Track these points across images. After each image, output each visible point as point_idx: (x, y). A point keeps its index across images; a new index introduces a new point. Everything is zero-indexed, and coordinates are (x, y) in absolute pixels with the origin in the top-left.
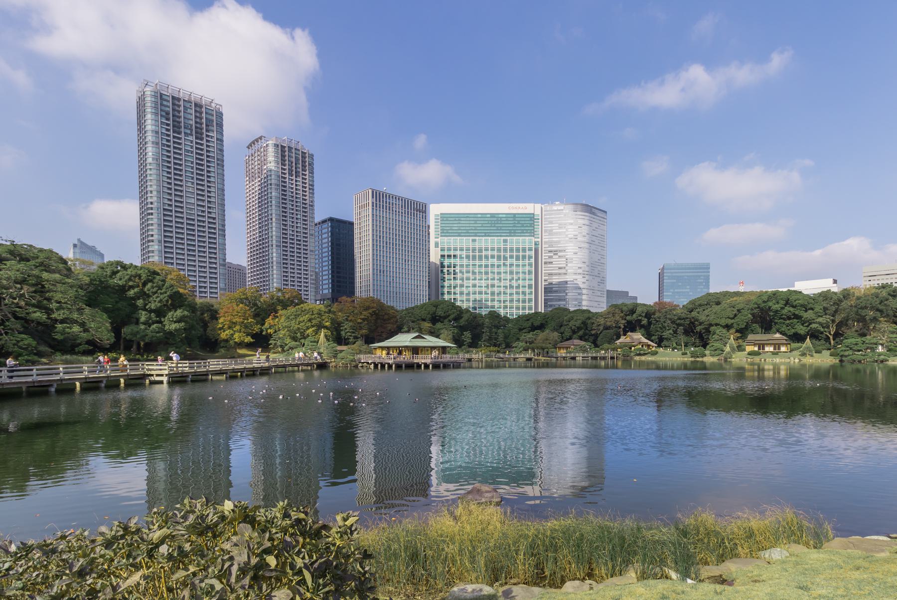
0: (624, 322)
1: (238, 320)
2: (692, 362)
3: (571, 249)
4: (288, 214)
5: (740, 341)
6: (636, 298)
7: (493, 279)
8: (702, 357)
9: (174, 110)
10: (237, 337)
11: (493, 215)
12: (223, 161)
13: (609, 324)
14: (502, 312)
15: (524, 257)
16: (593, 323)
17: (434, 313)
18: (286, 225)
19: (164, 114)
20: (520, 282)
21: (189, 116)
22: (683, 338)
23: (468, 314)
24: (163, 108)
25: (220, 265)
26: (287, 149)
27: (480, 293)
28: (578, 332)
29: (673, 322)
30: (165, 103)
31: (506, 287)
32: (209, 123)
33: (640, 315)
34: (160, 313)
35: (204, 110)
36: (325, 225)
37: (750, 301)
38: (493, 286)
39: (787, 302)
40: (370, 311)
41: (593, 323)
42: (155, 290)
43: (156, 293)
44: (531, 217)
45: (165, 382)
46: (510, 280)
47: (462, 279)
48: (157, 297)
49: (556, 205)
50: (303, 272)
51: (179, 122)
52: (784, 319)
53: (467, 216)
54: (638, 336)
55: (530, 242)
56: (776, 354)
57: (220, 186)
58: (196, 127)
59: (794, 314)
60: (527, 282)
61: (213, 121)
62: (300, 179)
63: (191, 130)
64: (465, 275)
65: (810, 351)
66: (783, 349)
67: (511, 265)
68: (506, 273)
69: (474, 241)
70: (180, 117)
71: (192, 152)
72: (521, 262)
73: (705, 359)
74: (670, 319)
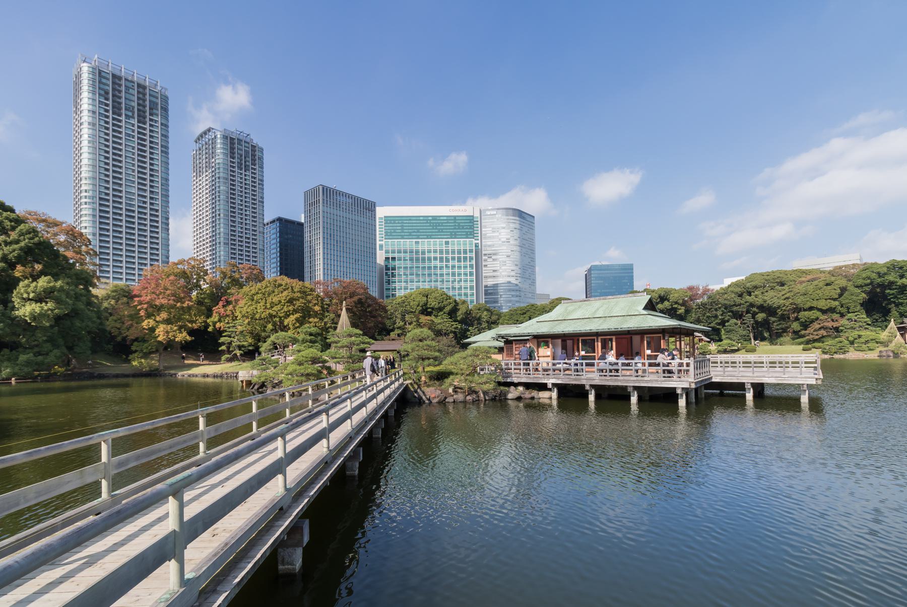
1: (164, 301)
4: (236, 210)
7: (436, 281)
8: (844, 353)
9: (114, 89)
10: (161, 334)
11: (435, 218)
17: (426, 304)
18: (234, 222)
19: (102, 92)
20: (463, 284)
21: (132, 97)
23: (465, 306)
24: (102, 86)
26: (236, 141)
30: (104, 81)
32: (153, 106)
35: (147, 91)
40: (356, 298)
44: (471, 220)
47: (406, 282)
55: (471, 244)
57: (164, 176)
58: (139, 110)
60: (469, 284)
61: (157, 104)
63: (133, 112)
67: (453, 267)
68: (448, 274)
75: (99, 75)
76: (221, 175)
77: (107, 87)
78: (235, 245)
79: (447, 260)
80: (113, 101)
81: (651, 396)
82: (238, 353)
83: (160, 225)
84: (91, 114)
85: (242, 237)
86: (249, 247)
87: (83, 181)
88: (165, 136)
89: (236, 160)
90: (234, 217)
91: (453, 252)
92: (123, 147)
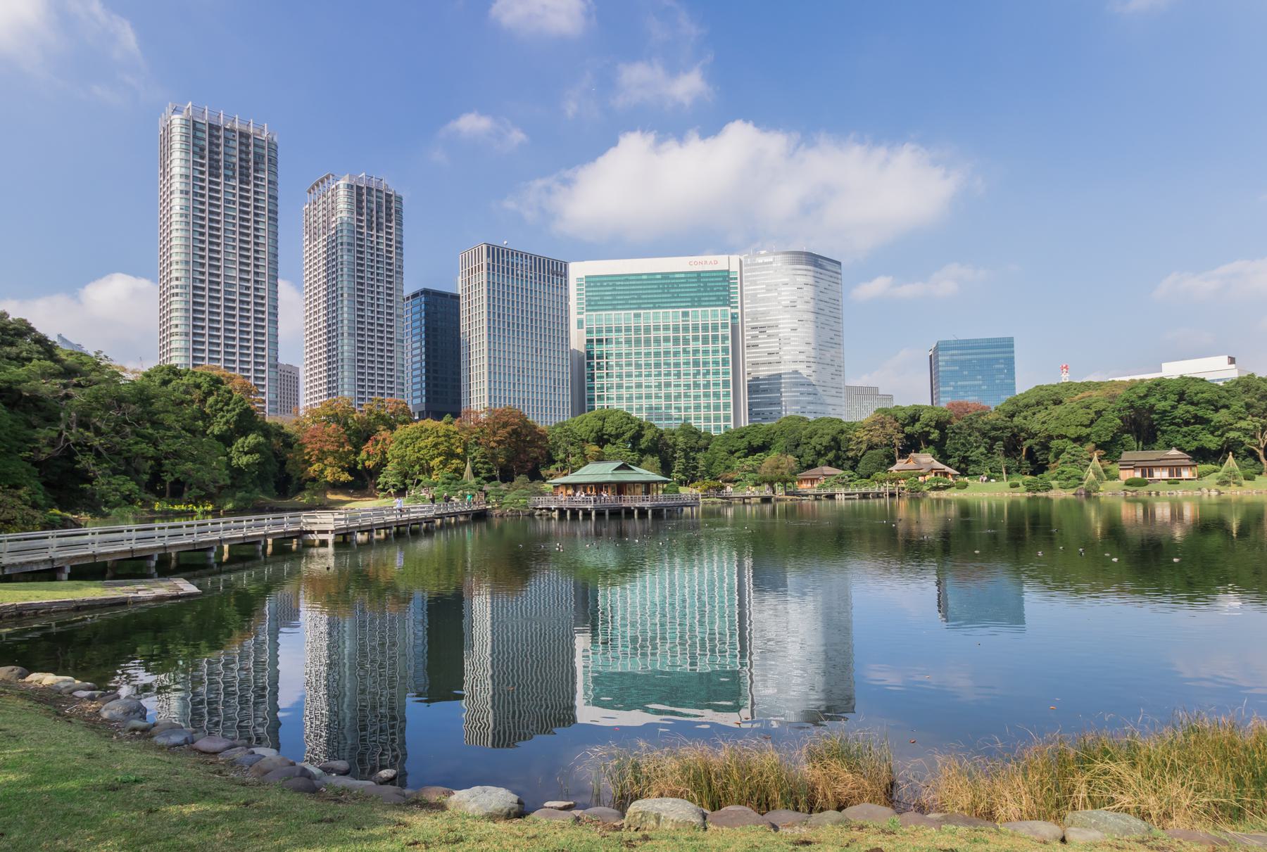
0: (901, 436)
2: (1029, 499)
3: (786, 322)
4: (366, 287)
5: (1105, 462)
6: (890, 397)
7: (668, 374)
8: (1047, 490)
9: (211, 143)
10: (329, 475)
11: (665, 276)
12: (276, 213)
13: (875, 440)
14: (701, 425)
15: (715, 338)
16: (850, 440)
17: (601, 430)
19: (197, 150)
20: (711, 378)
22: (1002, 461)
23: (652, 431)
24: (197, 142)
25: (270, 366)
26: (364, 191)
27: (649, 397)
28: (825, 454)
29: (984, 435)
30: (199, 134)
31: (688, 386)
33: (927, 425)
34: (226, 439)
35: (251, 141)
37: (1114, 397)
38: (668, 385)
39: (1181, 397)
40: (509, 429)
41: (850, 440)
42: (220, 405)
43: (221, 410)
44: (725, 276)
45: (330, 543)
46: (695, 375)
47: (620, 376)
48: (222, 417)
49: (760, 255)
50: (386, 372)
51: (218, 161)
52: (1178, 425)
53: (626, 278)
54: (926, 458)
55: (724, 315)
56: (1176, 482)
58: (241, 167)
59: (1195, 417)
60: (721, 378)
62: (383, 234)
64: (625, 369)
65: (1235, 477)
66: (1186, 474)
67: (696, 352)
68: (687, 363)
70: (218, 153)
72: (710, 347)
73: (1051, 494)
74: (979, 430)
75: (193, 127)
76: (345, 239)
77: (202, 143)
78: (363, 336)
79: (686, 341)
80: (210, 159)
81: (908, 542)
82: (392, 491)
84: (183, 180)
85: (372, 324)
86: (382, 332)
87: (174, 267)
88: (273, 198)
89: (364, 218)
90: (362, 297)
91: (695, 328)
92: (221, 218)
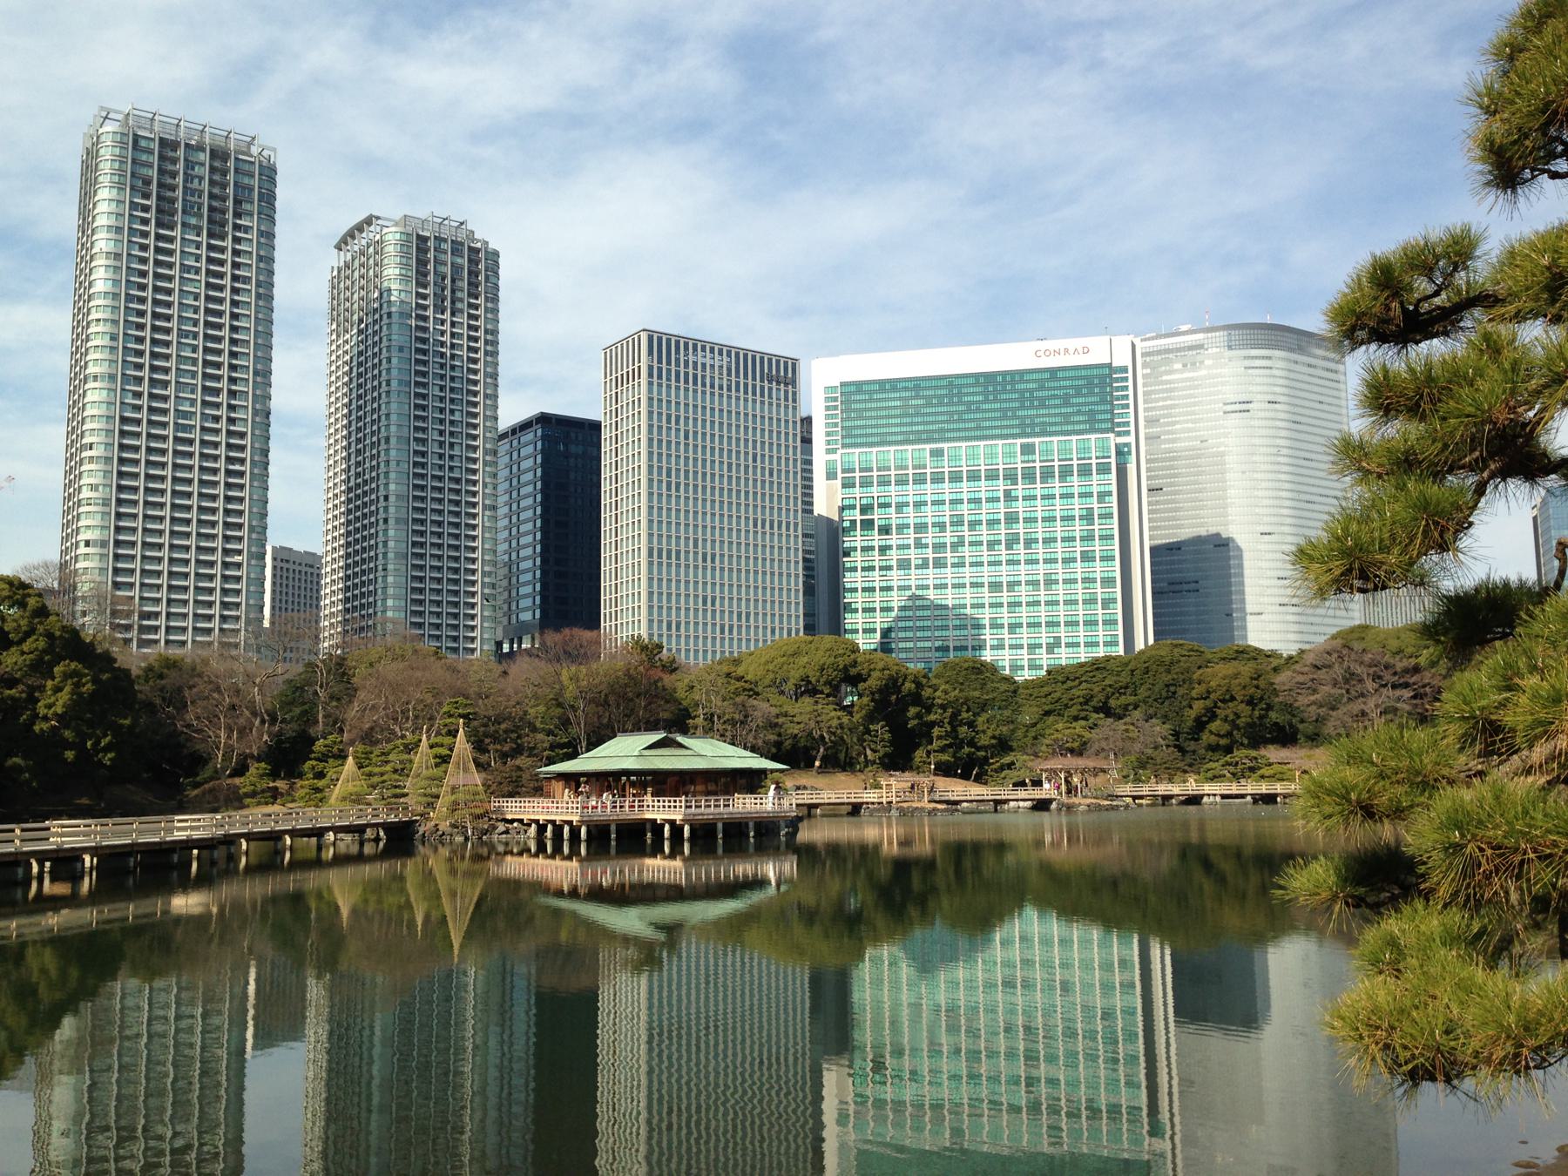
9: (161, 171)
35: (231, 164)
36: (528, 436)
61: (251, 189)
62: (462, 319)
69: (937, 454)
71: (194, 361)
83: (246, 480)
85: (440, 479)
88: (267, 260)
